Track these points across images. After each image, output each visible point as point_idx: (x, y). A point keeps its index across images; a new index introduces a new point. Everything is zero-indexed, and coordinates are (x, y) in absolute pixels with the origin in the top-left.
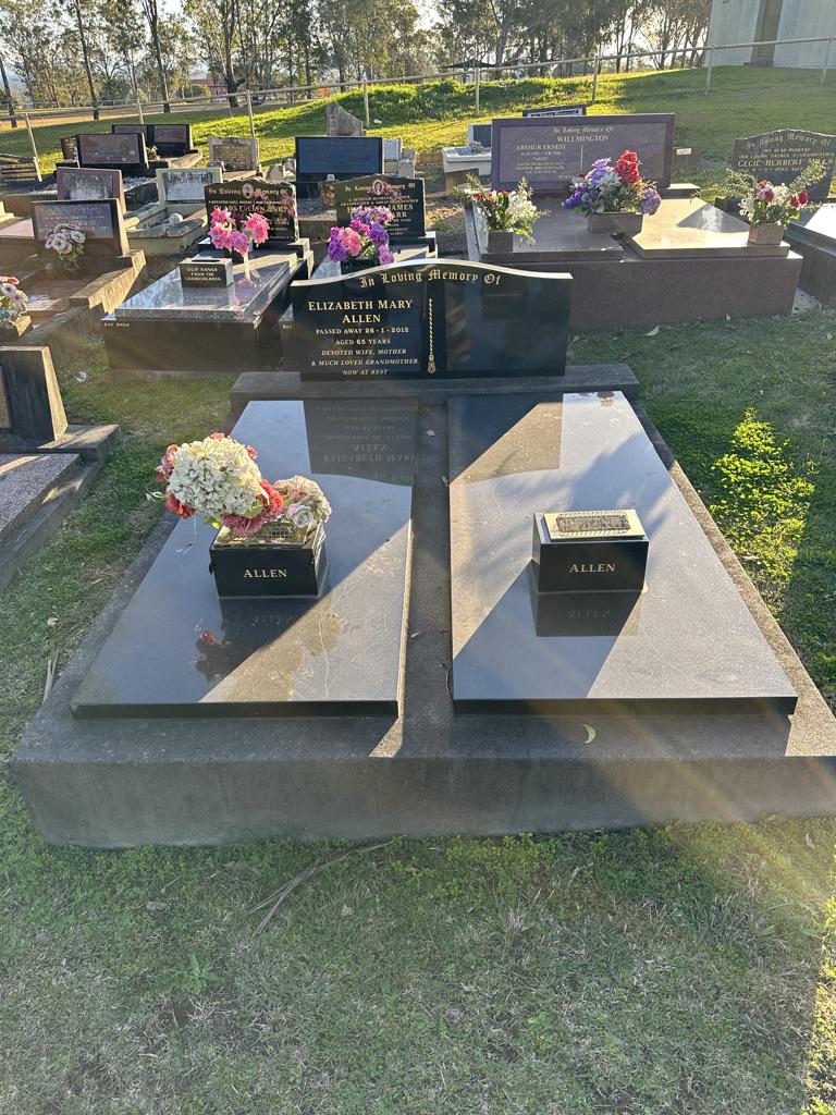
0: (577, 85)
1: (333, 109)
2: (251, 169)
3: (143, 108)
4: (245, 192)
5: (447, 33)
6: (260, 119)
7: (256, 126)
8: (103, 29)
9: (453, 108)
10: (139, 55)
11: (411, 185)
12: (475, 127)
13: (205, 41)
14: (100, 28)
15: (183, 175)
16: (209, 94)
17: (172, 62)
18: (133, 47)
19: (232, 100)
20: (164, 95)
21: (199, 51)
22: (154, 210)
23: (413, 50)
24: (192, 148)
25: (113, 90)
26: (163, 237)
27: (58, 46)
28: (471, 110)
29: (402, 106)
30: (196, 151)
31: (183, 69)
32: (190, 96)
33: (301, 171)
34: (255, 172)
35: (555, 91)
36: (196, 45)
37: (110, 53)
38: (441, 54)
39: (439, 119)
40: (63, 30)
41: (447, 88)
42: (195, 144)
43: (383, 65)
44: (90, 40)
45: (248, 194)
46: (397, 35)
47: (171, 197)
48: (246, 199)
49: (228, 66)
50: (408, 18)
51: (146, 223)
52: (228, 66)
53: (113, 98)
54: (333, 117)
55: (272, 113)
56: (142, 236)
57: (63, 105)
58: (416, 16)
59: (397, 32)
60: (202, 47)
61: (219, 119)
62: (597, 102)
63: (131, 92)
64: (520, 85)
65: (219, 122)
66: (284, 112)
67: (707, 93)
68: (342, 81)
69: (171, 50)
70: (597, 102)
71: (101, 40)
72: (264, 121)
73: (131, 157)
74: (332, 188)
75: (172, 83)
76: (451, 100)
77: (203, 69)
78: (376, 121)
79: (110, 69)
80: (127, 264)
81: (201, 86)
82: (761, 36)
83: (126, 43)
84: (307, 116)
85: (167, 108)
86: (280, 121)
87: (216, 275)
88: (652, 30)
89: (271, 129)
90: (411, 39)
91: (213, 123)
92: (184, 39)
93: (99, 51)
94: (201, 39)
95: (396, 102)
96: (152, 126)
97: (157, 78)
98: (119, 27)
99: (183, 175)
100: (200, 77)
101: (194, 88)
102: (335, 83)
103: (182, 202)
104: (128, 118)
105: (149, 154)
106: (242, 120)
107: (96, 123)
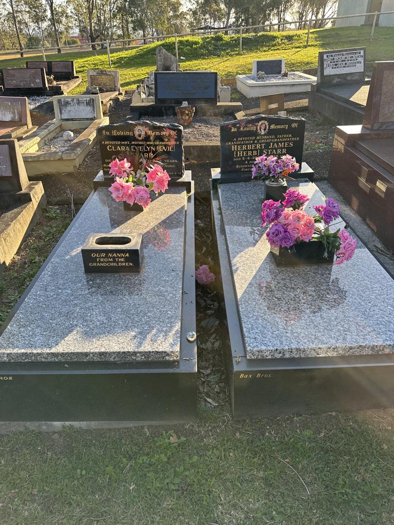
0: (293, 36)
1: (160, 51)
2: (115, 91)
3: (45, 52)
4: (137, 133)
5: (195, 13)
6: (114, 57)
7: (112, 61)
8: (27, 12)
9: (225, 50)
10: (45, 25)
11: (294, 125)
12: (258, 62)
13: (76, 17)
14: (25, 12)
15: (73, 100)
16: (79, 43)
17: (61, 28)
18: (42, 20)
19: (93, 46)
20: (58, 44)
21: (74, 22)
22: (52, 128)
23: (178, 22)
24: (75, 75)
25: (33, 42)
26: (59, 159)
27: (4, 20)
28: (237, 51)
29: (196, 49)
30: (78, 77)
31: (67, 31)
32: (70, 44)
33: (159, 97)
34: (117, 93)
35: (282, 40)
36: (72, 19)
37: (31, 24)
38: (191, 24)
39: (219, 56)
40: (7, 12)
41: (219, 39)
42: (77, 72)
43: (165, 29)
44: (20, 17)
45: (140, 136)
46: (171, 14)
47: (65, 116)
48: (138, 140)
49: (91, 29)
50: (176, 6)
51: (46, 139)
52: (91, 29)
53: (33, 46)
54: (160, 56)
55: (121, 53)
56: (42, 159)
57: (8, 49)
58: (181, 4)
59: (171, 12)
60: (76, 20)
61: (89, 57)
62: (309, 46)
63: (41, 43)
64: (260, 36)
65: (89, 59)
66: (126, 52)
67: (371, 40)
68: (144, 36)
69: (61, 22)
70: (309, 46)
71: (26, 17)
72: (116, 58)
73: (37, 83)
74: (187, 112)
75: (61, 38)
76: (222, 45)
77: (76, 32)
78: (182, 58)
79: (31, 31)
80: (27, 199)
81: (75, 39)
82: (370, 9)
83: (38, 19)
84: (141, 55)
85: (59, 50)
86: (125, 58)
87: (127, 260)
88: (294, 11)
89: (120, 63)
90: (178, 16)
91: (86, 59)
92: (67, 17)
93: (25, 23)
94: (75, 16)
95: (192, 47)
96: (51, 62)
97: (54, 36)
98: (34, 11)
99: (73, 100)
100: (75, 35)
101: (72, 40)
102: (139, 38)
103: (72, 120)
104: (34, 57)
105: (49, 82)
106: (103, 58)
107: (22, 59)
